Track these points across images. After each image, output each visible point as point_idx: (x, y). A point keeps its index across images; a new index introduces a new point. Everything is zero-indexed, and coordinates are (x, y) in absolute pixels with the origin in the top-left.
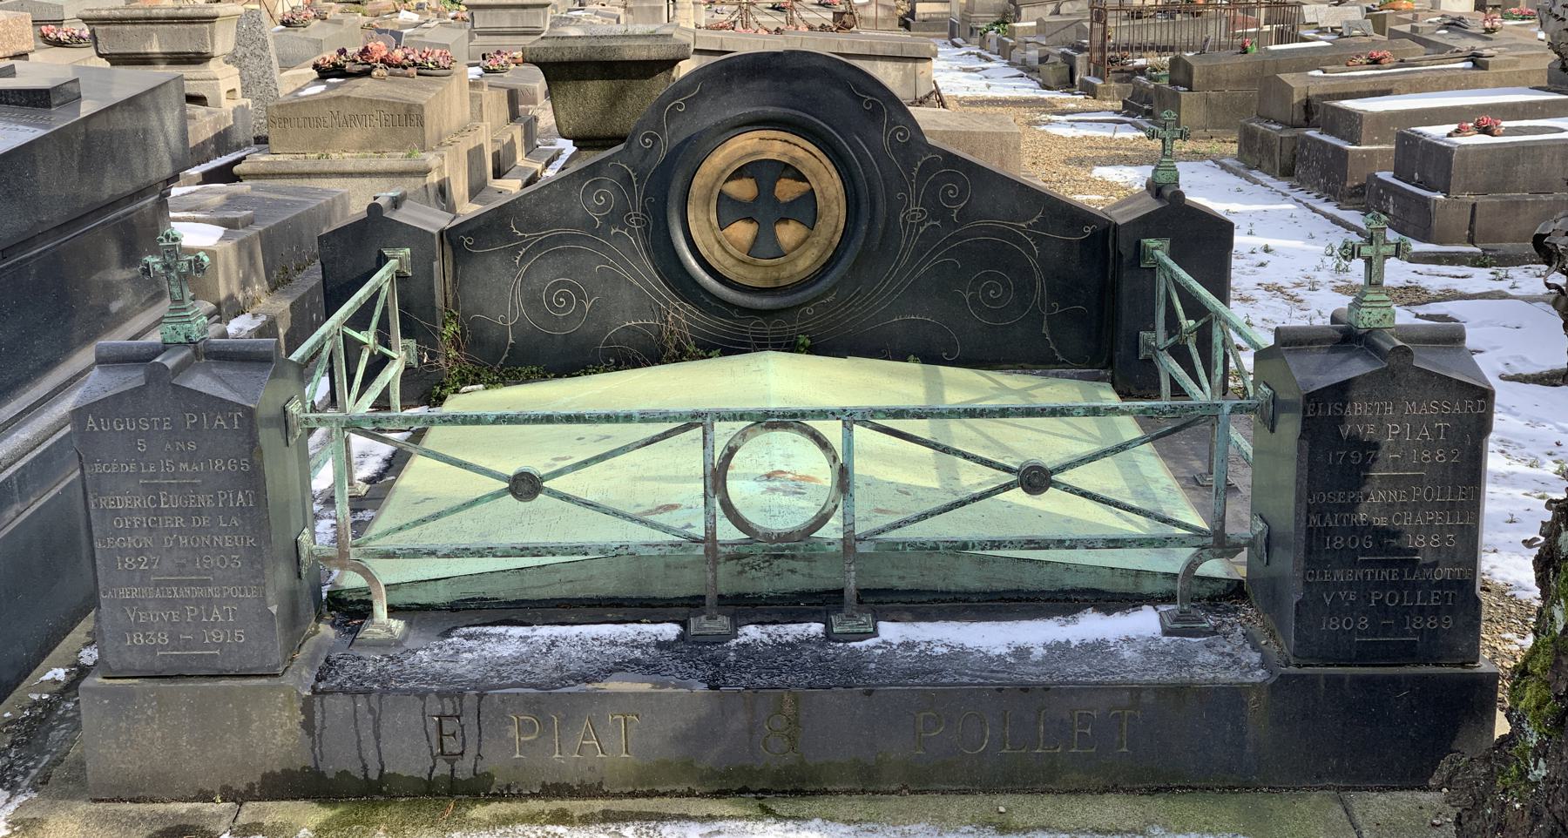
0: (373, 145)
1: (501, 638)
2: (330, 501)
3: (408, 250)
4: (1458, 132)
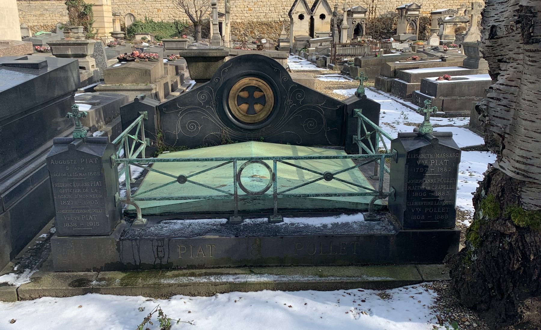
0: (135, 81)
1: (175, 223)
2: (124, 185)
4: (439, 79)
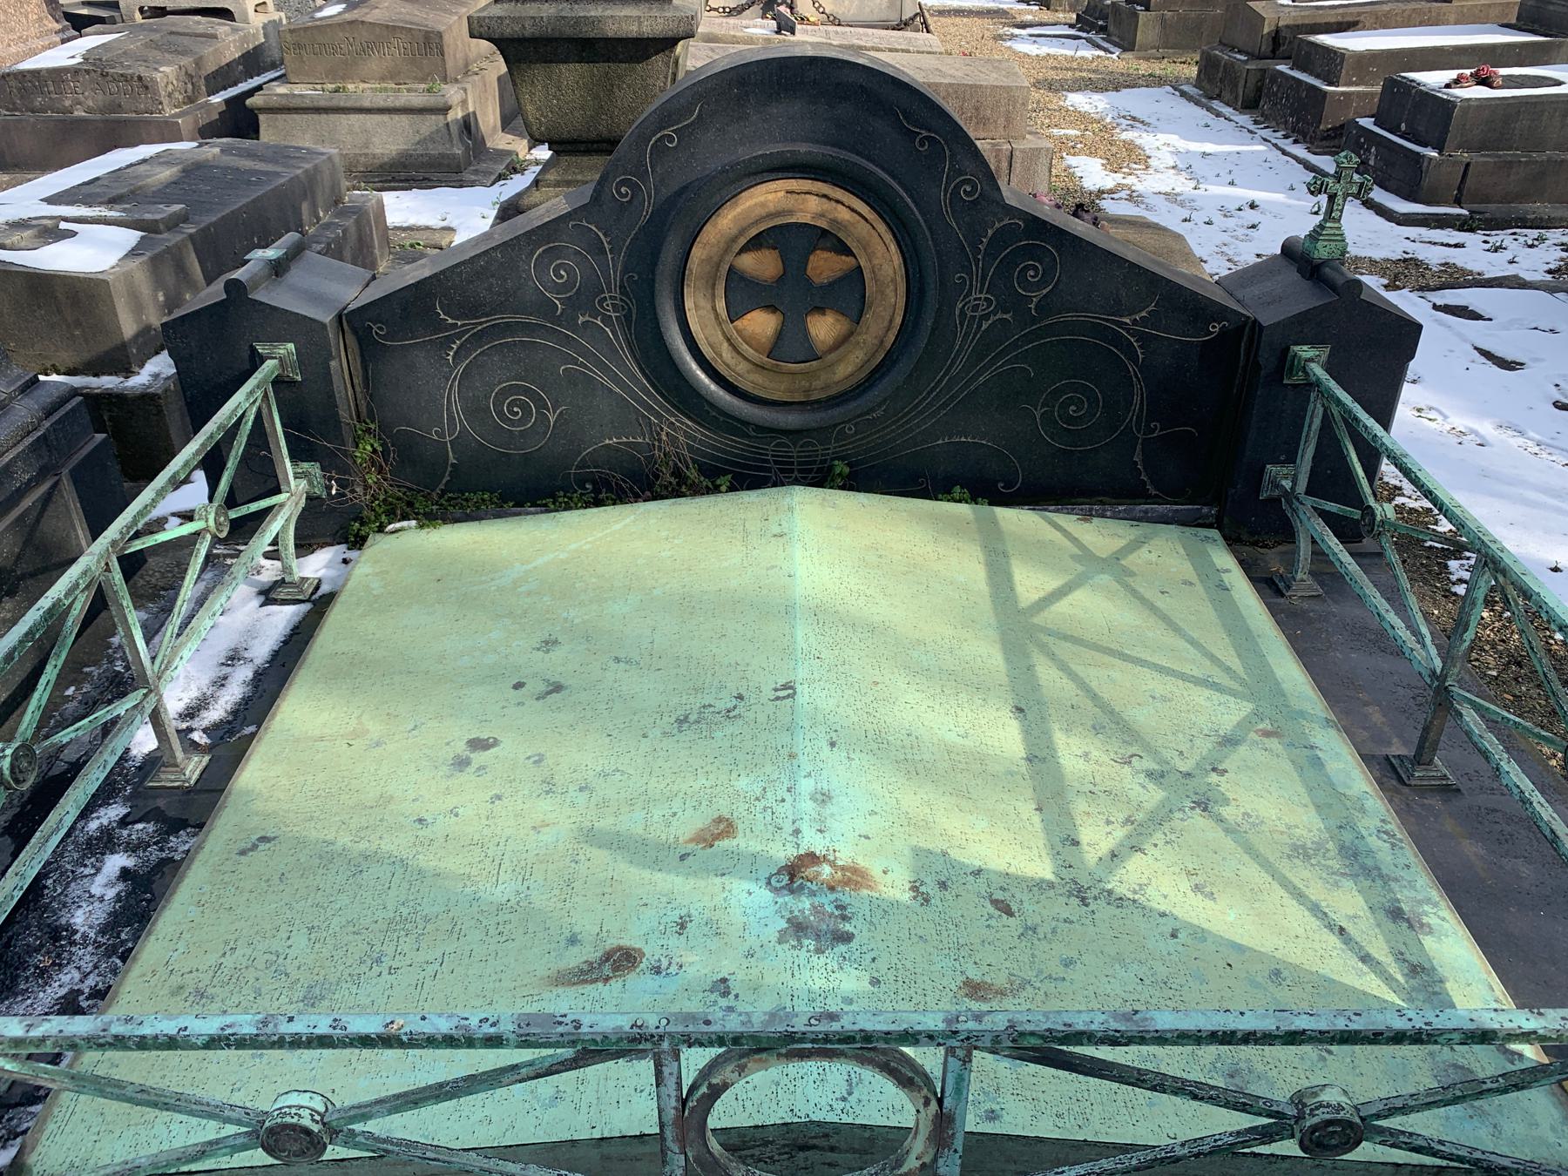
0: (392, 75)
3: (291, 346)
